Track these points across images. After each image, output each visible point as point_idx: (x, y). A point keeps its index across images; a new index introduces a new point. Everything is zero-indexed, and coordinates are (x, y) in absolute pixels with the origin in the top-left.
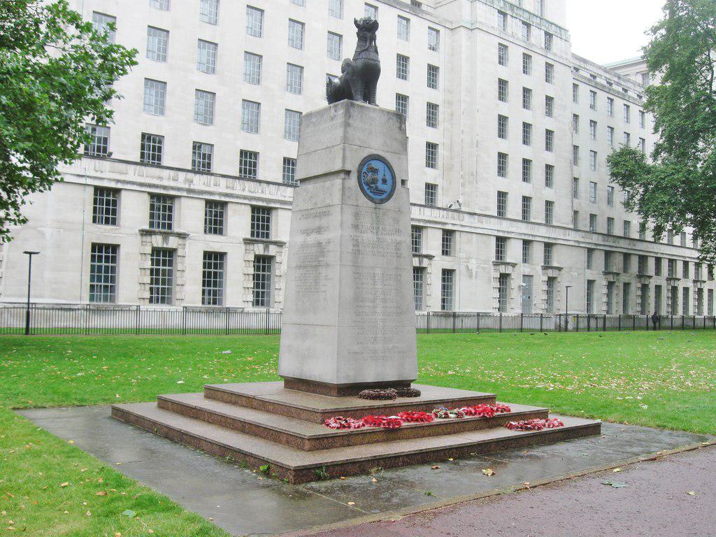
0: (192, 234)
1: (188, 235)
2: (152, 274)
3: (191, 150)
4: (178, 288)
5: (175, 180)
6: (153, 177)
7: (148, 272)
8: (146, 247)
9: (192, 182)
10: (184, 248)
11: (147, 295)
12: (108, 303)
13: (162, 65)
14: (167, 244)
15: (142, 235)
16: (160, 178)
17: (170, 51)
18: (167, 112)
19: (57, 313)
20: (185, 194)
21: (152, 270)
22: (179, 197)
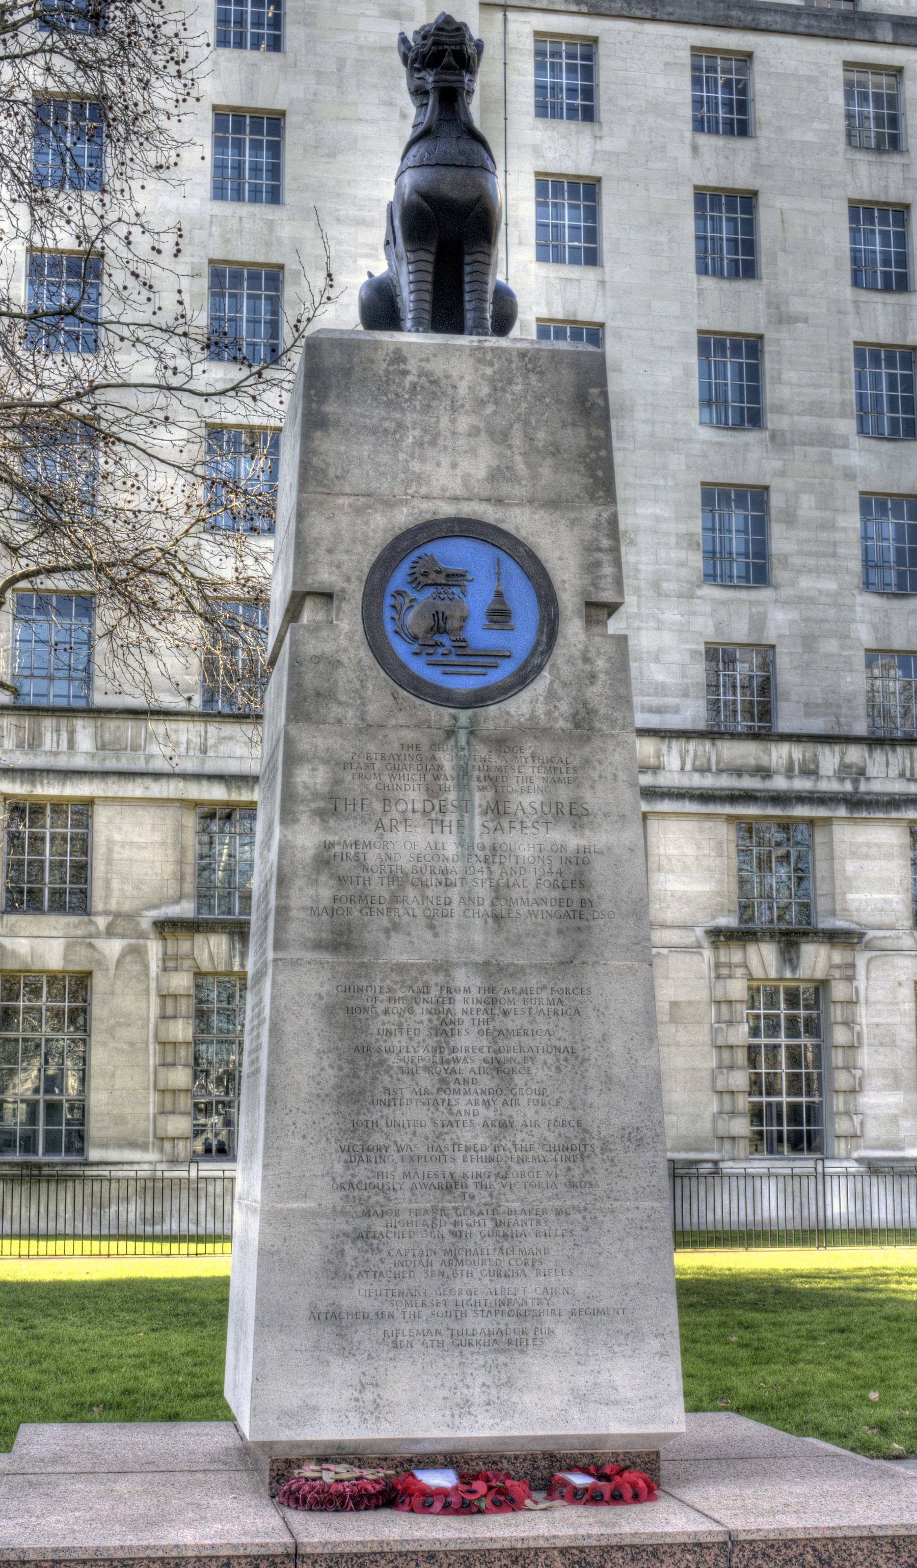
0: (871, 934)
1: (861, 935)
2: (753, 1062)
3: (844, 224)
4: (839, 1103)
5: (810, 771)
6: (738, 772)
7: (741, 1057)
8: (271, 396)
9: (862, 772)
10: (850, 979)
11: (741, 1127)
12: (62, 1157)
13: (750, 437)
14: (794, 968)
15: (715, 945)
16: (764, 772)
17: (772, 394)
18: (778, 574)
19: (52, 1225)
20: (842, 812)
21: (752, 1052)
22: (828, 821)
